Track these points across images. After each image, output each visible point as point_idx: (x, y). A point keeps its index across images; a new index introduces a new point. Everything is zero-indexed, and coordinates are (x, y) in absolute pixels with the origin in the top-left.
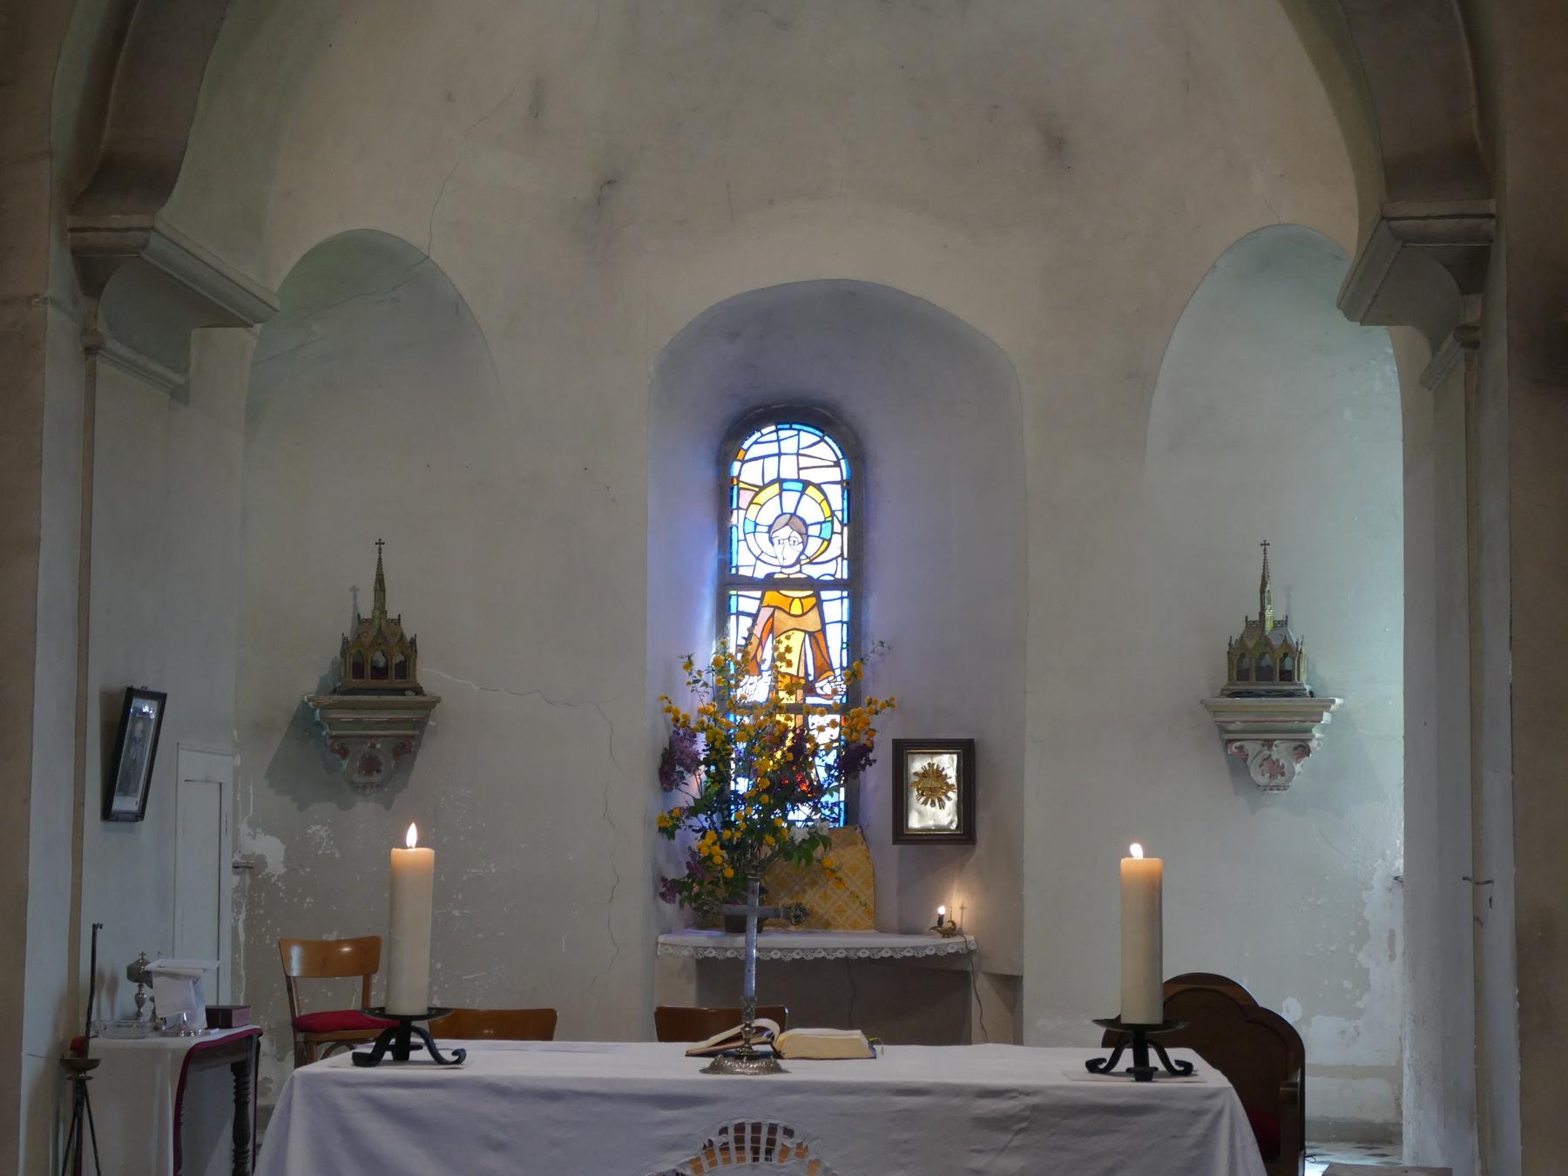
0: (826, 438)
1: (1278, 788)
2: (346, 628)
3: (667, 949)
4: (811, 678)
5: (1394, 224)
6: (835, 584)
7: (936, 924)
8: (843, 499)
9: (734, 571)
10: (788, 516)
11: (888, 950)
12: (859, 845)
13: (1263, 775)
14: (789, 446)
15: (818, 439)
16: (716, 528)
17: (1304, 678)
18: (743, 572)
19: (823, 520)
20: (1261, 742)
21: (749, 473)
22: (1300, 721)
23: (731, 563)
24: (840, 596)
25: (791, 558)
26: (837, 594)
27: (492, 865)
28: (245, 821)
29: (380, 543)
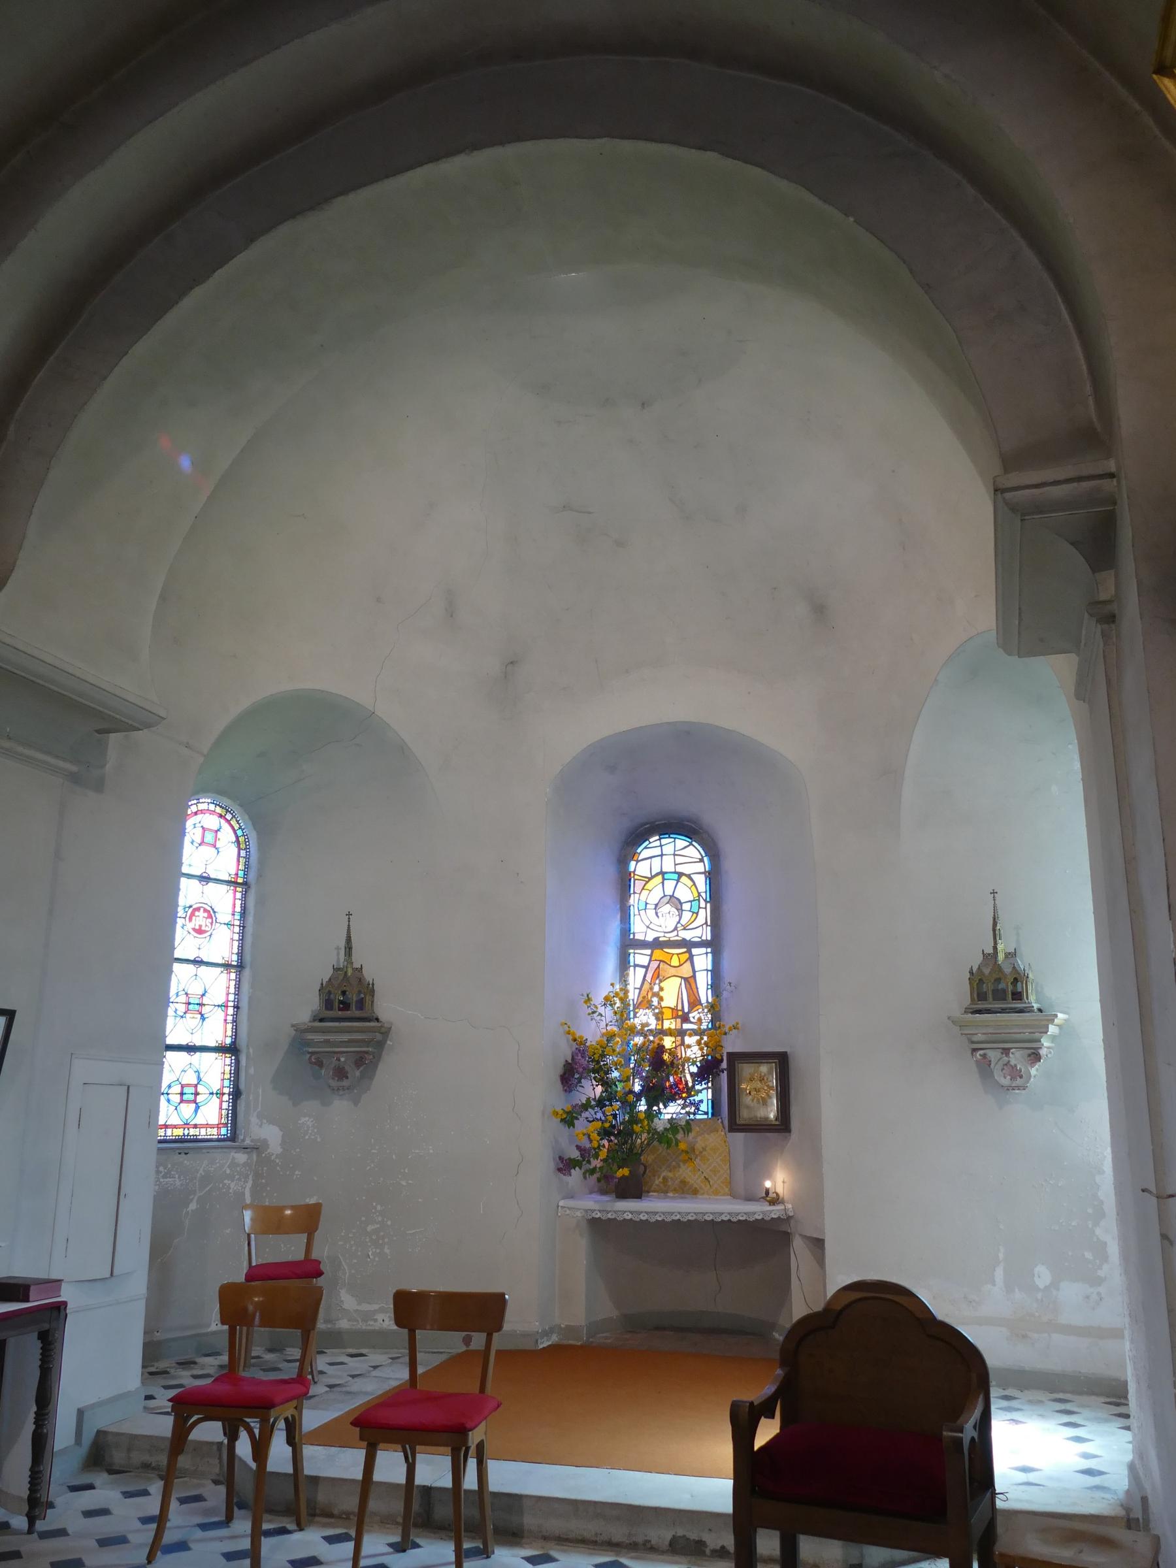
0: (694, 843)
1: (1018, 1088)
2: (327, 974)
3: (566, 1211)
4: (686, 1010)
5: (1008, 495)
6: (702, 944)
7: (764, 1195)
8: (706, 884)
9: (632, 936)
10: (669, 897)
12: (720, 1132)
13: (1005, 1077)
14: (668, 849)
15: (688, 844)
17: (1032, 998)
18: (639, 937)
19: (692, 899)
20: (1000, 1050)
21: (640, 868)
22: (1030, 1033)
23: (630, 931)
26: (703, 950)
27: (431, 1147)
28: (255, 1114)
29: (349, 914)
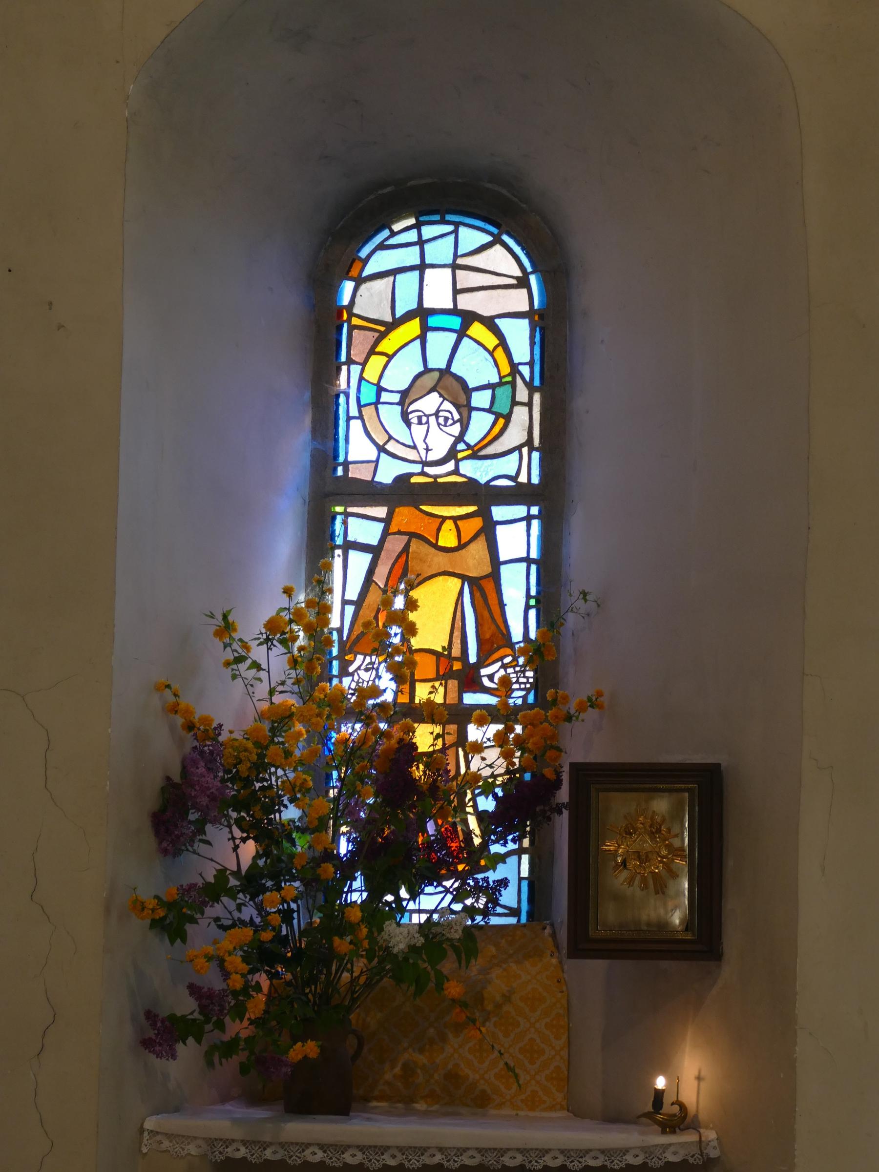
0: (505, 238)
3: (161, 1143)
4: (473, 659)
7: (649, 1108)
8: (532, 344)
9: (340, 471)
10: (436, 375)
11: (557, 1154)
16: (307, 395)
23: (336, 456)
24: (525, 514)
25: (440, 445)
26: (520, 511)
